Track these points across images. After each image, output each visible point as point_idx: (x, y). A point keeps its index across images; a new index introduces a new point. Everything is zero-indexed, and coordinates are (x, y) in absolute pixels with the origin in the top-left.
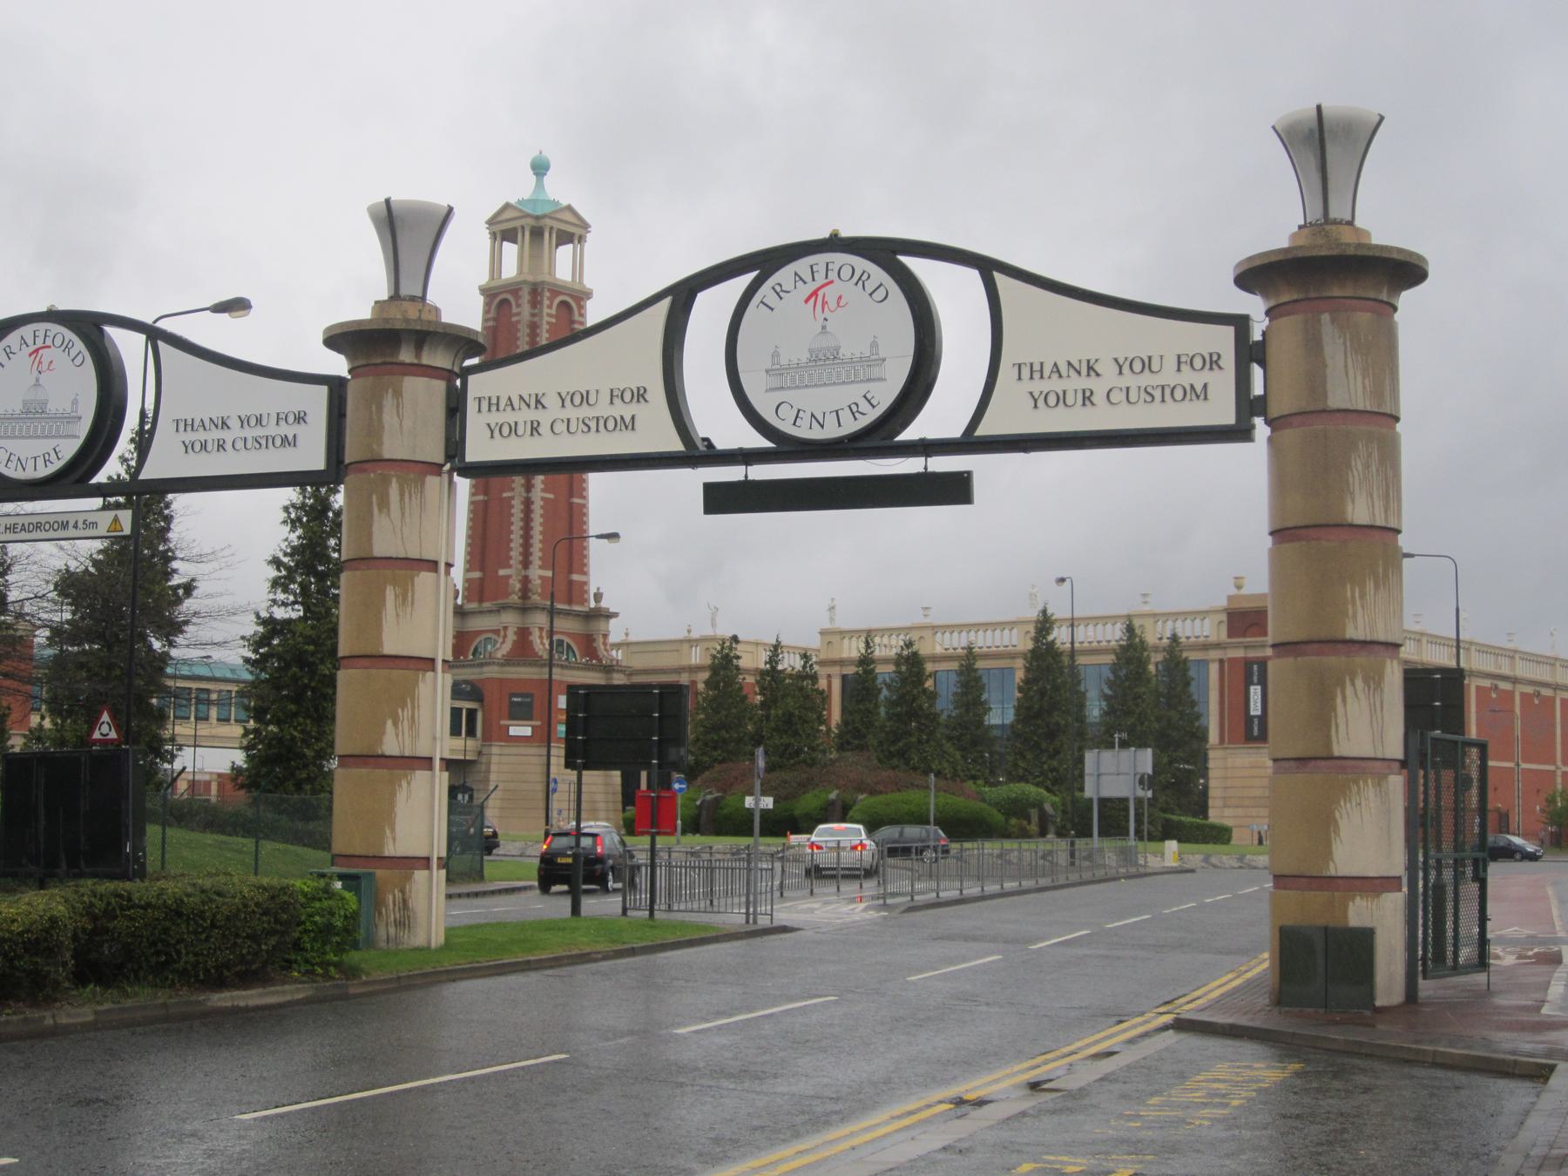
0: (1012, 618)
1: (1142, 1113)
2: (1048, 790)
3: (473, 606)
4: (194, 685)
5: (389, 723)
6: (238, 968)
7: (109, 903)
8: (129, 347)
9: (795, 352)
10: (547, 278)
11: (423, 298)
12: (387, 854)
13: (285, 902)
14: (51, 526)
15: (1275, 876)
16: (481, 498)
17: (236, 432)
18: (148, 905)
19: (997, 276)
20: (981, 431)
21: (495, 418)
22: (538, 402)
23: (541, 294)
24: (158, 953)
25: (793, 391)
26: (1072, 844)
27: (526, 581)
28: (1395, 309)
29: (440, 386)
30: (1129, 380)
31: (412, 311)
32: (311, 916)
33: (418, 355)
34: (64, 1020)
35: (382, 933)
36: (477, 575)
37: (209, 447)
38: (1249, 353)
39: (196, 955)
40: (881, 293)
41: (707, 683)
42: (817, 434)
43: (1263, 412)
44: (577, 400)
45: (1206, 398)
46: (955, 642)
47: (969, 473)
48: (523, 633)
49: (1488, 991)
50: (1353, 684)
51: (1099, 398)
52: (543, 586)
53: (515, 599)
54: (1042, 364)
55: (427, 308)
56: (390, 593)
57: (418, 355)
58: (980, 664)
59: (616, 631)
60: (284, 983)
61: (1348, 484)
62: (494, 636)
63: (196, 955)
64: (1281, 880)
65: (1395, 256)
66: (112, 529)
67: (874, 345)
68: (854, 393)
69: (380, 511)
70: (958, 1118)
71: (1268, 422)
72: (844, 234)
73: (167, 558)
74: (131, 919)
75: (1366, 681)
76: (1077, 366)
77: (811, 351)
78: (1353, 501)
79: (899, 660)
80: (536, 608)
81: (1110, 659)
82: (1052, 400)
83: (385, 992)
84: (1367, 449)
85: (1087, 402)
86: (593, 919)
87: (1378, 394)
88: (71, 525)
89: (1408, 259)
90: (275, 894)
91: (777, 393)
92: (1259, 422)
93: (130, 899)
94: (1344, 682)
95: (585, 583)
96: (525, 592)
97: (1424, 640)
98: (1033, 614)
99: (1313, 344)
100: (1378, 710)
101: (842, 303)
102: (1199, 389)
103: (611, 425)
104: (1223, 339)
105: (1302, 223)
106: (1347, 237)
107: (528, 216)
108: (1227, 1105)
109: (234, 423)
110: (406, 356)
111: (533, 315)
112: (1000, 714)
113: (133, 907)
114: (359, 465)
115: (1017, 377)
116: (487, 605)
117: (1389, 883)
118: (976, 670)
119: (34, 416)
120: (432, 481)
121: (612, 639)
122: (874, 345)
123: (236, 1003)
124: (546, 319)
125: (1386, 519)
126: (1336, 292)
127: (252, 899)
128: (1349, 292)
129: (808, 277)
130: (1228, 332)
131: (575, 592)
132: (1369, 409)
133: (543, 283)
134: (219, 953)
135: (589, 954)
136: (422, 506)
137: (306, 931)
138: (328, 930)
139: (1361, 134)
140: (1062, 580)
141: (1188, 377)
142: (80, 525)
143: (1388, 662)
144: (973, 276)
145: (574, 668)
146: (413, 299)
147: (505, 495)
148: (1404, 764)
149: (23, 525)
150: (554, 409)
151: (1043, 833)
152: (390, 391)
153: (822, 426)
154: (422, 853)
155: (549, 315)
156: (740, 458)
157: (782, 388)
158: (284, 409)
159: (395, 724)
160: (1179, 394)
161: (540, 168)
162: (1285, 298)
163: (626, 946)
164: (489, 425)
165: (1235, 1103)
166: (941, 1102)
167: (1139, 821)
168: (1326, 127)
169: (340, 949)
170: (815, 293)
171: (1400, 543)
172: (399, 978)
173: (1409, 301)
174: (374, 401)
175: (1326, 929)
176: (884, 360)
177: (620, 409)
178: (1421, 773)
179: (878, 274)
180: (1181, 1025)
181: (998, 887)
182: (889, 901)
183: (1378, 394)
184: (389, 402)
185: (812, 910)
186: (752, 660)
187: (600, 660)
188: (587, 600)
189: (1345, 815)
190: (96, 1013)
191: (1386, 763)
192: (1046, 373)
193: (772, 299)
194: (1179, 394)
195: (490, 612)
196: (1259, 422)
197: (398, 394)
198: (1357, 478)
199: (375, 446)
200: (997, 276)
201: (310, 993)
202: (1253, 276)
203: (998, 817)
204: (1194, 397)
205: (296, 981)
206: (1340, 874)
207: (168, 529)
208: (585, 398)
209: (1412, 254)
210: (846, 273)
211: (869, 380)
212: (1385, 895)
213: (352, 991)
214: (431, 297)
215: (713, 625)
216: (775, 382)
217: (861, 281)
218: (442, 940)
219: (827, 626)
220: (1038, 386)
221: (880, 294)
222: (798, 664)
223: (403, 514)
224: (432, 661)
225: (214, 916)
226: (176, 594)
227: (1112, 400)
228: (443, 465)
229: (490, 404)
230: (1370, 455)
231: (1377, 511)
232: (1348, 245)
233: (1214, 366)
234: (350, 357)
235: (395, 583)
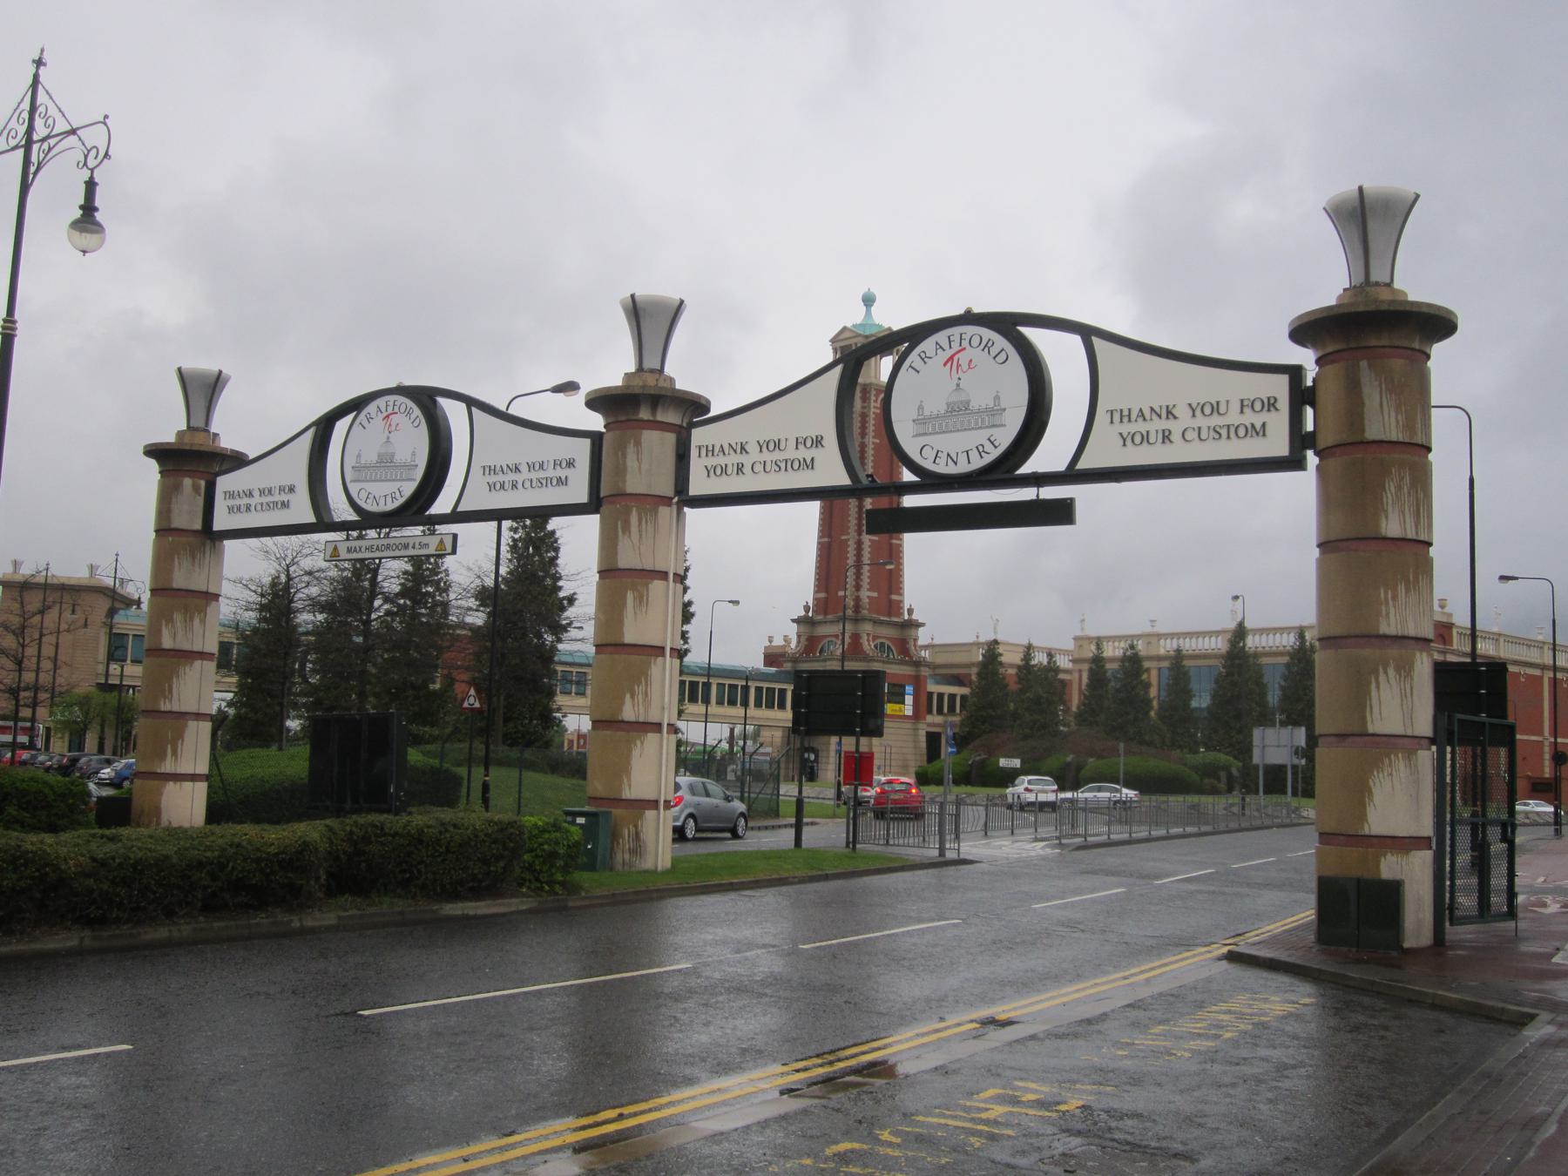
0: (1219, 628)
1: (1136, 1042)
2: (1235, 757)
3: (820, 617)
4: (574, 670)
5: (628, 696)
6: (471, 884)
7: (366, 832)
8: (455, 413)
9: (937, 406)
10: (873, 381)
11: (661, 370)
12: (624, 797)
13: (511, 834)
14: (397, 547)
15: (1321, 834)
16: (826, 540)
17: (525, 474)
18: (396, 834)
19: (1095, 340)
20: (1081, 465)
21: (711, 462)
22: (1169, 412)
23: (870, 392)
24: (403, 871)
25: (940, 436)
26: (1243, 799)
27: (857, 600)
28: (1428, 357)
29: (671, 438)
30: (1201, 421)
31: (651, 380)
32: (541, 844)
33: (654, 412)
34: (309, 922)
35: (619, 858)
36: (822, 595)
37: (506, 487)
38: (1301, 396)
39: (434, 873)
41: (979, 674)
42: (951, 469)
43: (1313, 446)
44: (771, 446)
45: (1264, 435)
46: (1166, 647)
47: (1072, 500)
48: (856, 637)
49: (1516, 937)
50: (1386, 672)
51: (1176, 437)
52: (870, 603)
53: (849, 612)
54: (1130, 410)
55: (663, 377)
56: (630, 596)
57: (654, 412)
58: (1186, 663)
59: (923, 637)
60: (513, 896)
61: (1382, 504)
62: (834, 639)
63: (434, 873)
64: (1325, 837)
65: (1425, 310)
67: (997, 398)
68: (980, 437)
69: (623, 533)
70: (974, 1038)
71: (1317, 453)
72: (976, 310)
73: (557, 578)
74: (382, 844)
75: (1398, 670)
76: (1158, 410)
77: (948, 404)
78: (1387, 517)
79: (1124, 659)
80: (864, 619)
81: (1286, 659)
82: (1138, 439)
83: (602, 905)
84: (1400, 474)
85: (1166, 440)
86: (808, 850)
87: (1410, 426)
88: (411, 545)
89: (1437, 313)
90: (503, 827)
91: (920, 438)
92: (1310, 454)
93: (382, 829)
94: (1377, 670)
95: (902, 601)
96: (857, 608)
97: (1502, 640)
98: (1232, 625)
99: (1353, 387)
100: (1409, 695)
102: (1258, 427)
103: (796, 465)
104: (1279, 386)
105: (1348, 286)
106: (1385, 295)
107: (860, 335)
108: (1217, 1037)
109: (524, 468)
110: (644, 414)
111: (863, 408)
112: (1201, 701)
113: (385, 835)
114: (610, 499)
116: (830, 617)
117: (1418, 842)
118: (1183, 666)
119: (386, 465)
120: (665, 513)
121: (921, 642)
123: (466, 912)
124: (872, 410)
125: (1417, 533)
126: (1373, 342)
127: (482, 830)
128: (1384, 342)
129: (946, 346)
130: (1283, 381)
131: (894, 607)
132: (1401, 439)
133: (870, 384)
134: (453, 872)
135: (787, 878)
136: (655, 530)
137: (537, 856)
138: (553, 855)
140: (1236, 598)
141: (1250, 418)
142: (417, 546)
143: (1418, 654)
144: (1075, 340)
145: (892, 663)
146: (652, 371)
147: (843, 537)
148: (1433, 741)
150: (754, 454)
151: (1230, 790)
152: (632, 441)
153: (956, 463)
154: (652, 797)
155: (875, 407)
156: (892, 490)
157: (925, 434)
158: (559, 457)
159: (632, 697)
160: (1242, 432)
161: (869, 301)
162: (1330, 349)
163: (820, 873)
164: (706, 467)
165: (1228, 1035)
166: (972, 1021)
167: (1295, 781)
168: (1367, 206)
169: (565, 869)
170: (951, 358)
171: (1431, 554)
172: (614, 895)
173: (1441, 354)
174: (621, 448)
175: (1358, 881)
176: (1004, 410)
177: (804, 453)
178: (1449, 749)
179: (1000, 342)
180: (1233, 957)
181: (1165, 831)
182: (1064, 841)
183: (1410, 426)
184: (631, 450)
185: (1000, 847)
186: (1011, 657)
187: (911, 657)
188: (903, 614)
189: (1378, 784)
190: (340, 918)
191: (1416, 741)
192: (1134, 417)
193: (918, 364)
194: (1242, 432)
195: (832, 622)
196: (1310, 454)
197: (638, 443)
198: (1390, 502)
199: (620, 485)
200: (1095, 340)
201: (534, 905)
202: (1304, 332)
203: (1195, 777)
204: (1254, 434)
205: (524, 895)
206: (1373, 833)
207: (556, 558)
208: (777, 445)
209: (1440, 308)
210: (976, 341)
211: (994, 426)
212: (1414, 852)
213: (571, 904)
214: (668, 370)
215: (995, 633)
217: (987, 347)
218: (668, 865)
219: (1079, 633)
220: (1127, 428)
221: (1002, 357)
222: (1045, 661)
223: (641, 536)
224: (662, 649)
225: (449, 843)
226: (562, 604)
227: (1186, 437)
228: (672, 499)
229: (1129, 416)
230: (1402, 479)
231: (1408, 527)
232: (1383, 301)
233: (1272, 409)
234: (605, 415)
235: (634, 589)
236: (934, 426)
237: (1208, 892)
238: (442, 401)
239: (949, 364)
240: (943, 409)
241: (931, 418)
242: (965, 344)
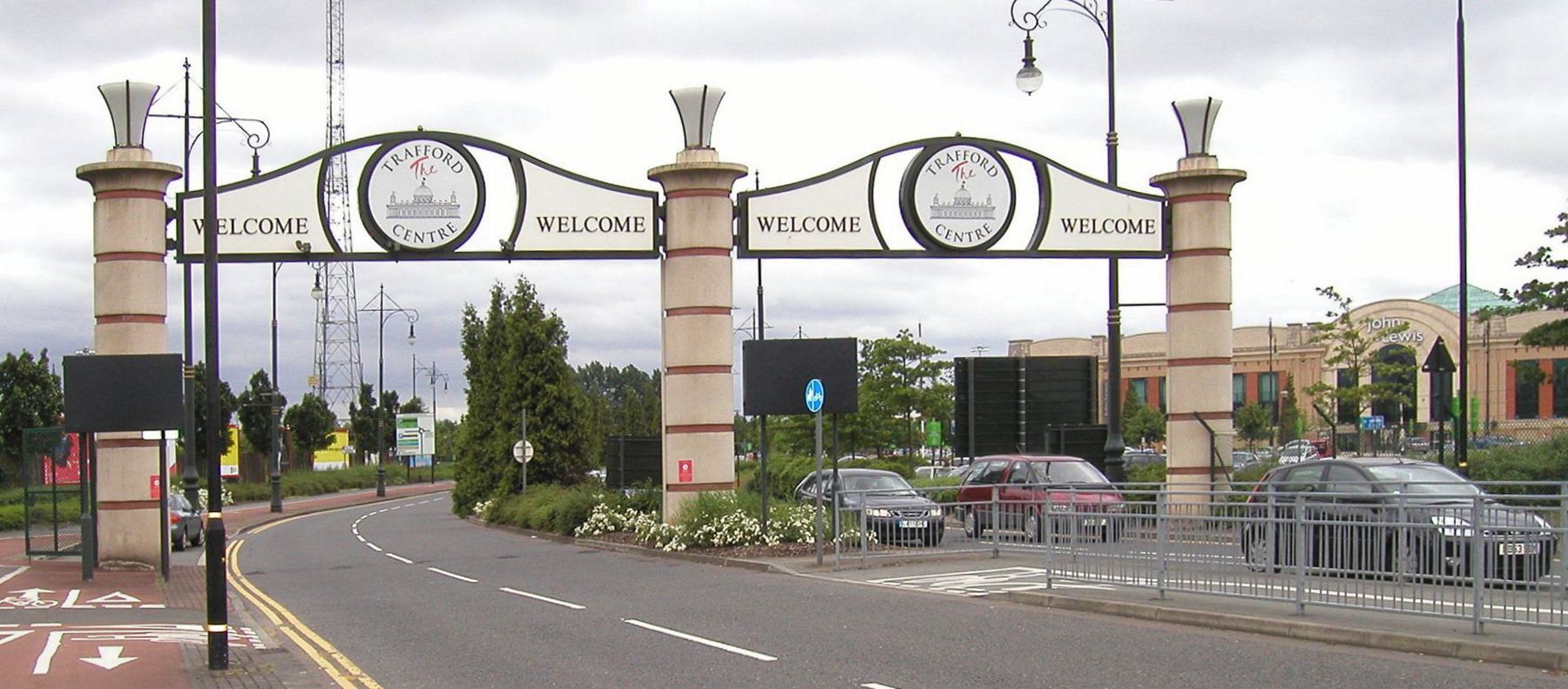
9: (947, 199)
40: (459, 167)
42: (419, 245)
67: (989, 199)
77: (955, 199)
91: (934, 220)
115: (576, 220)
122: (453, 197)
129: (414, 154)
170: (417, 163)
176: (994, 208)
210: (975, 158)
211: (986, 218)
217: (447, 159)
221: (458, 168)
236: (404, 212)
237: (1271, 392)
238: (1050, 167)
239: (956, 171)
241: (943, 207)
242: (968, 158)
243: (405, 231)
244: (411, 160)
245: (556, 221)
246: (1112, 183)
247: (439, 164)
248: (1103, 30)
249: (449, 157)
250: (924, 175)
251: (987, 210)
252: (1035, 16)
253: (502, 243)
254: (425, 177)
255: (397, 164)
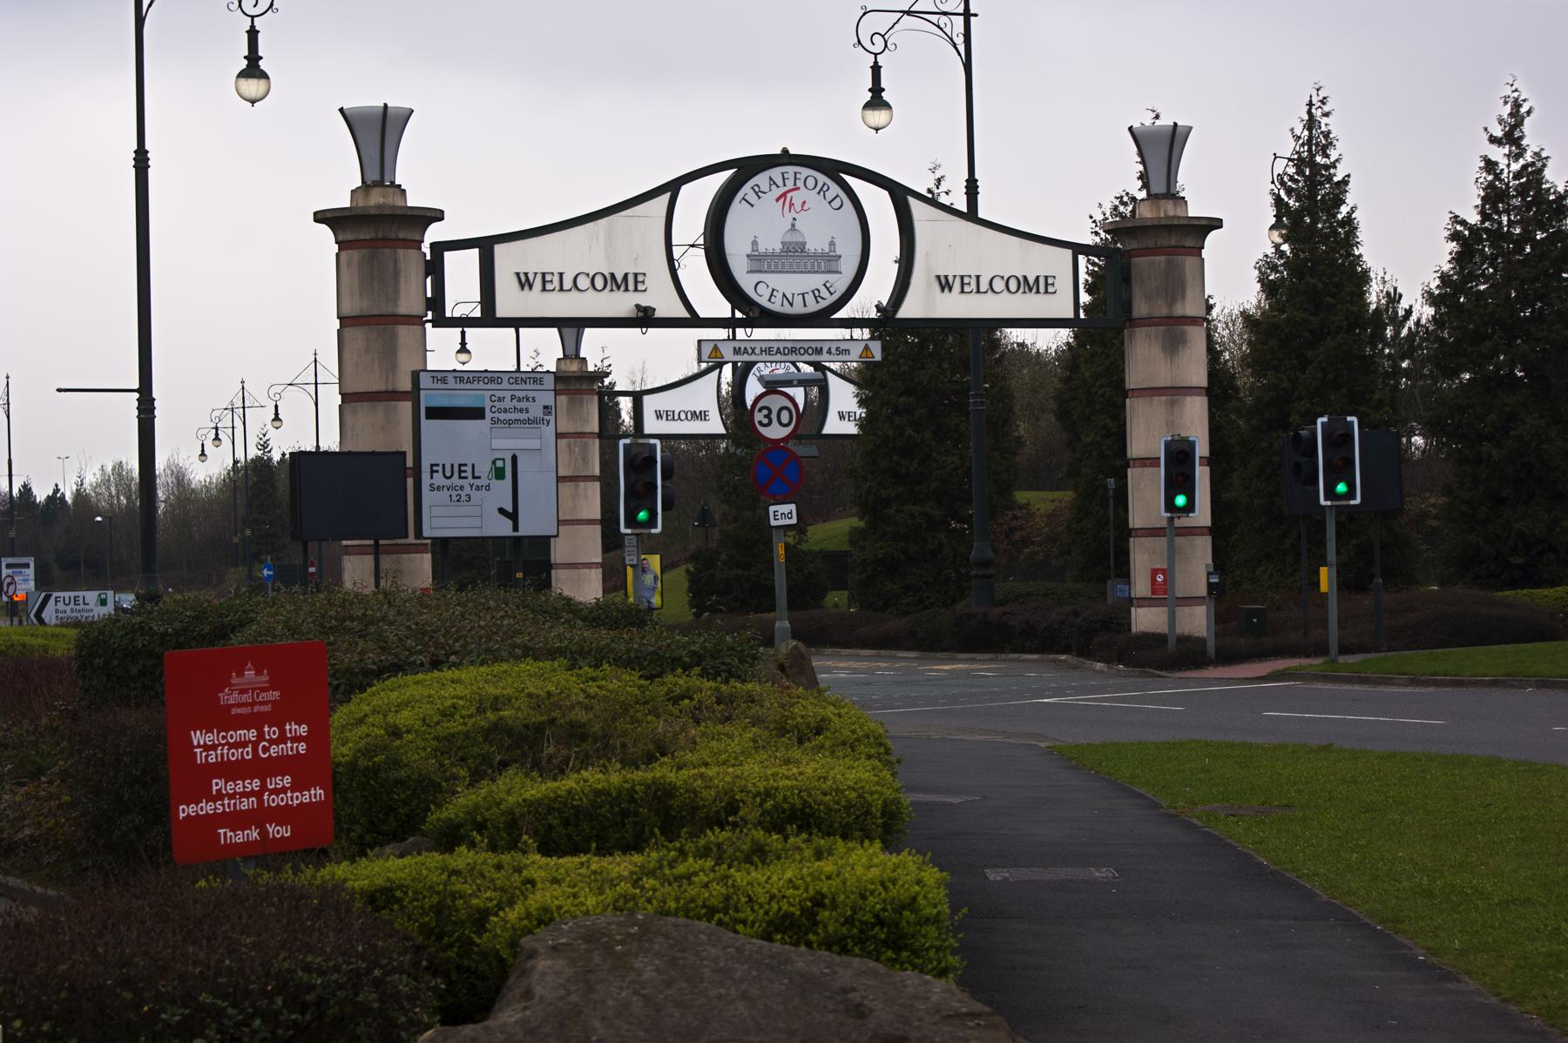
31: (1169, 209)
42: (787, 309)
66: (864, 355)
67: (832, 244)
68: (815, 281)
88: (825, 351)
101: (805, 208)
129: (780, 182)
139: (1175, 139)
142: (833, 351)
149: (778, 348)
170: (784, 195)
193: (752, 197)
210: (811, 183)
216: (756, 266)
217: (823, 191)
221: (836, 203)
239: (782, 200)
240: (778, 247)
243: (770, 290)
244: (778, 192)
245: (539, 278)
246: (971, 215)
247: (812, 197)
248: (959, 54)
249: (756, 188)
250: (737, 209)
251: (827, 261)
252: (883, 36)
253: (879, 308)
254: (796, 216)
255: (759, 197)
